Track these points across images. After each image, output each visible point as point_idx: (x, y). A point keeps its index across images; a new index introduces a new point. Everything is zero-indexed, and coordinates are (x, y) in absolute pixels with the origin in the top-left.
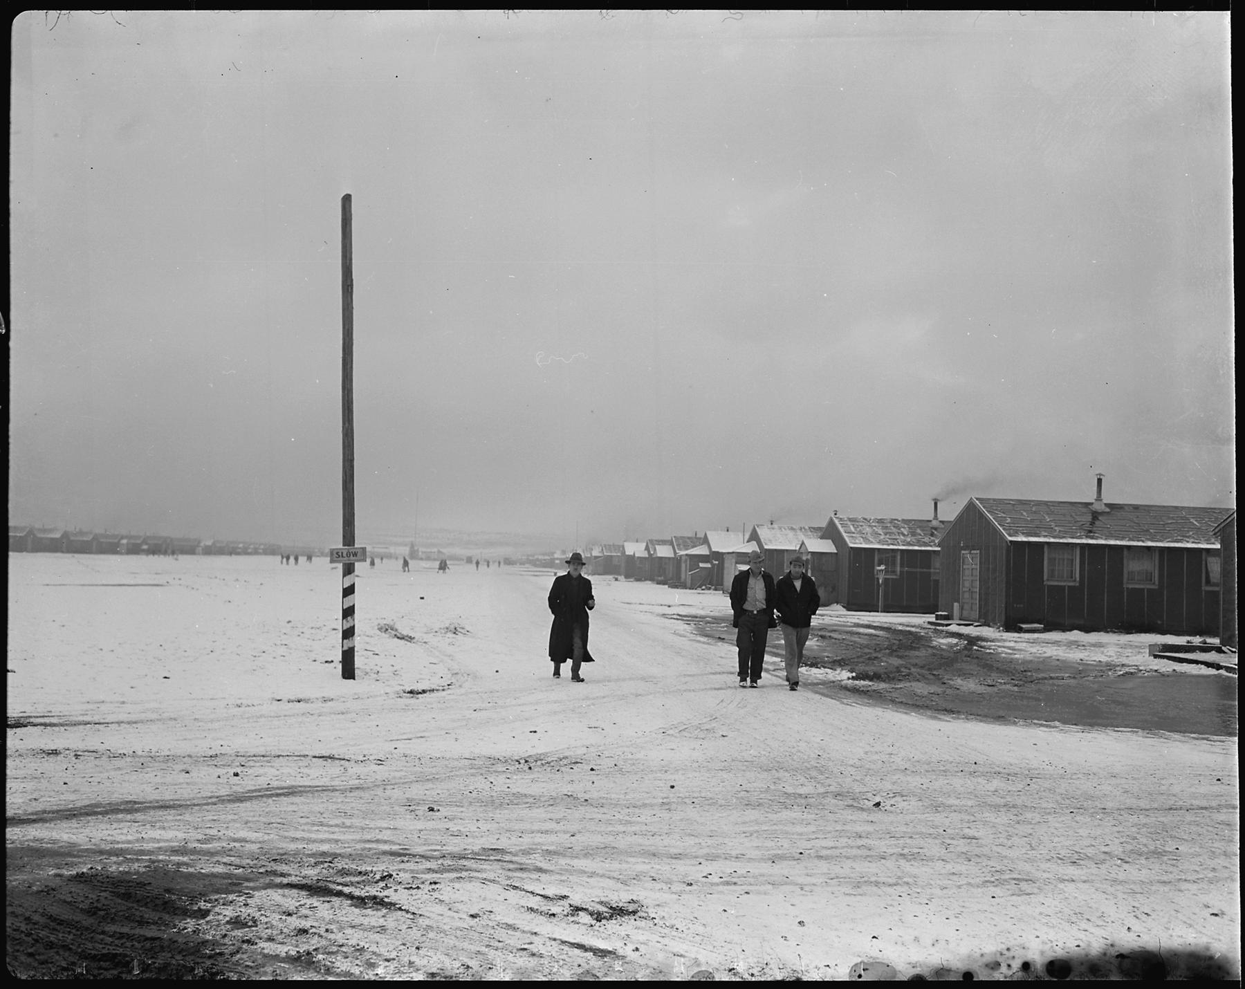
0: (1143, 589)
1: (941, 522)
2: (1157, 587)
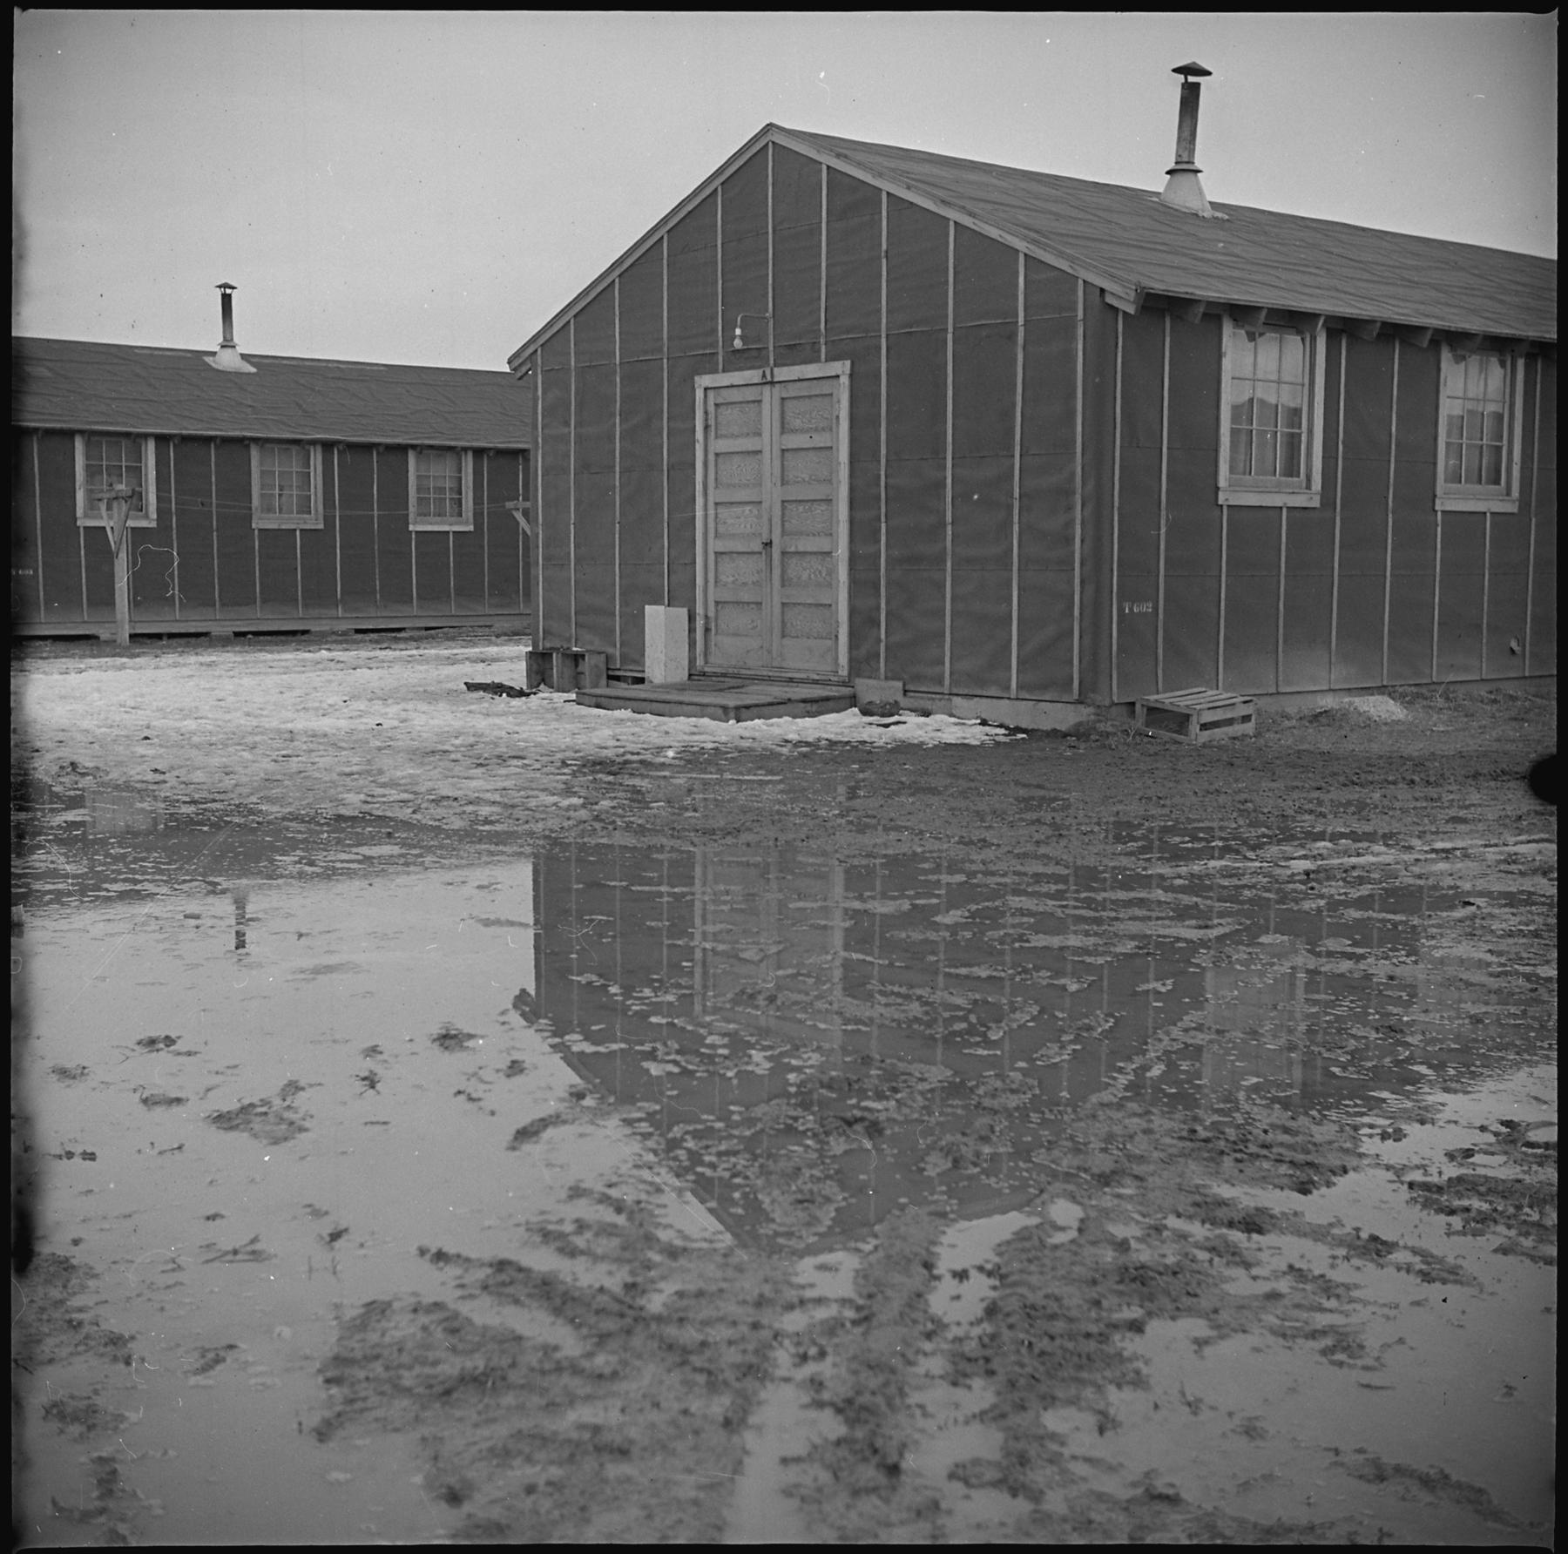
1: (244, 357)
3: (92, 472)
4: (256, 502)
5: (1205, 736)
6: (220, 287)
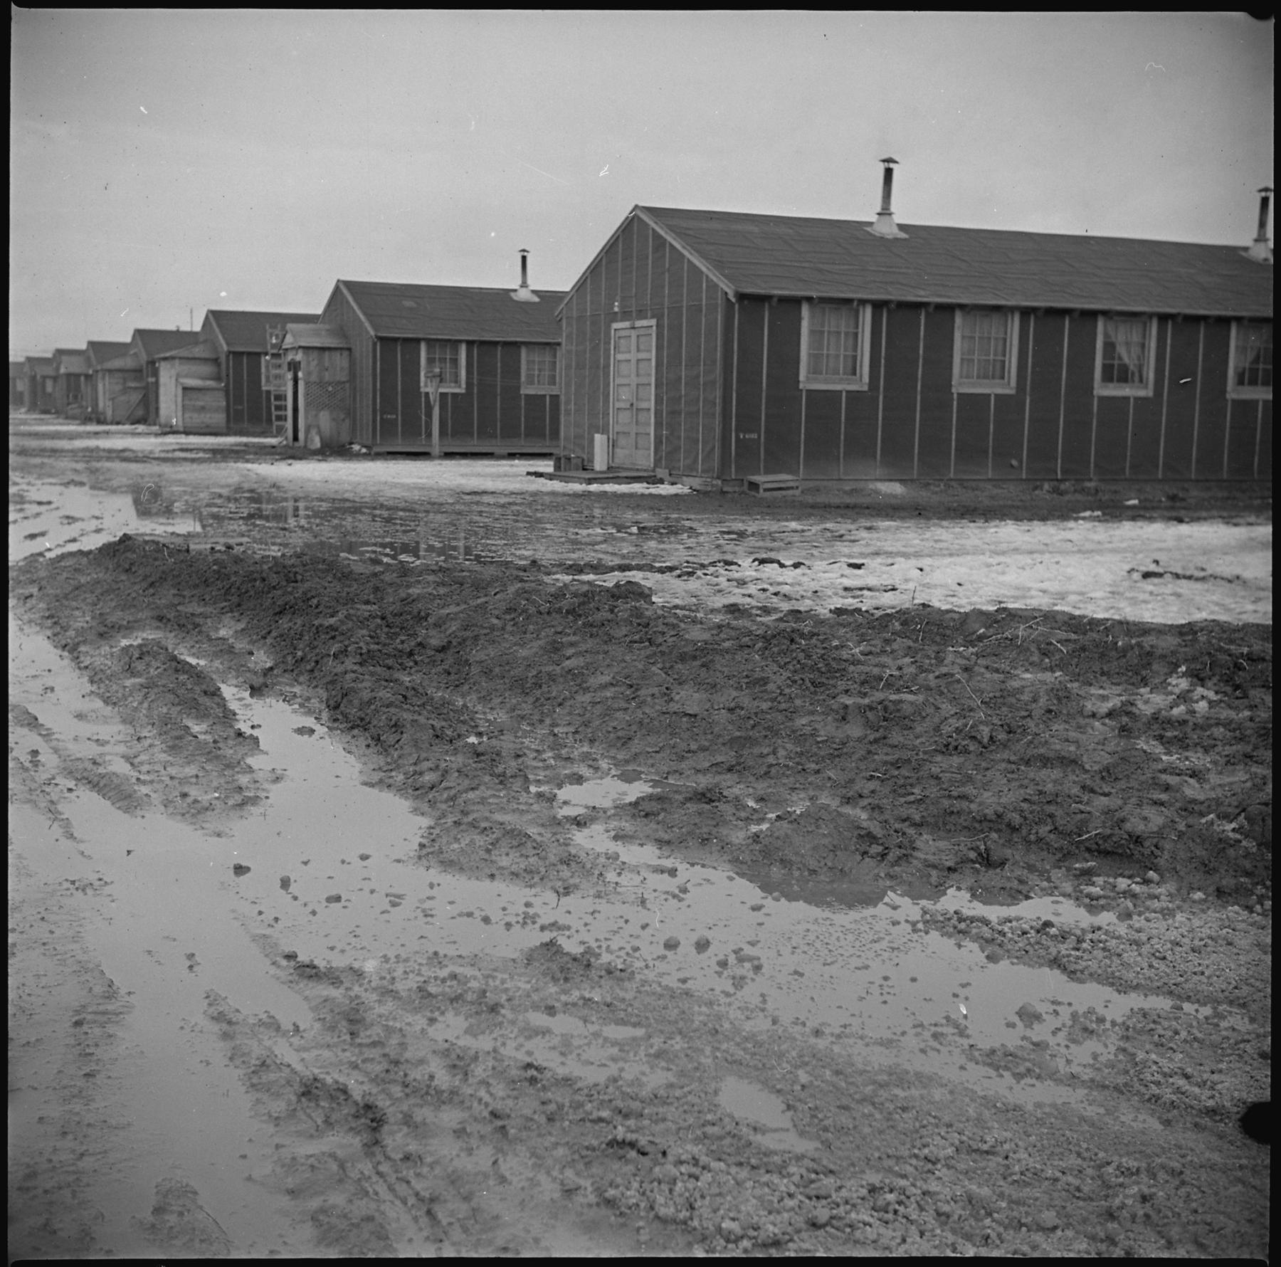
0: (1126, 399)
1: (533, 292)
2: (1013, 392)
3: (430, 361)
4: (523, 379)
5: (768, 494)
6: (884, 161)
